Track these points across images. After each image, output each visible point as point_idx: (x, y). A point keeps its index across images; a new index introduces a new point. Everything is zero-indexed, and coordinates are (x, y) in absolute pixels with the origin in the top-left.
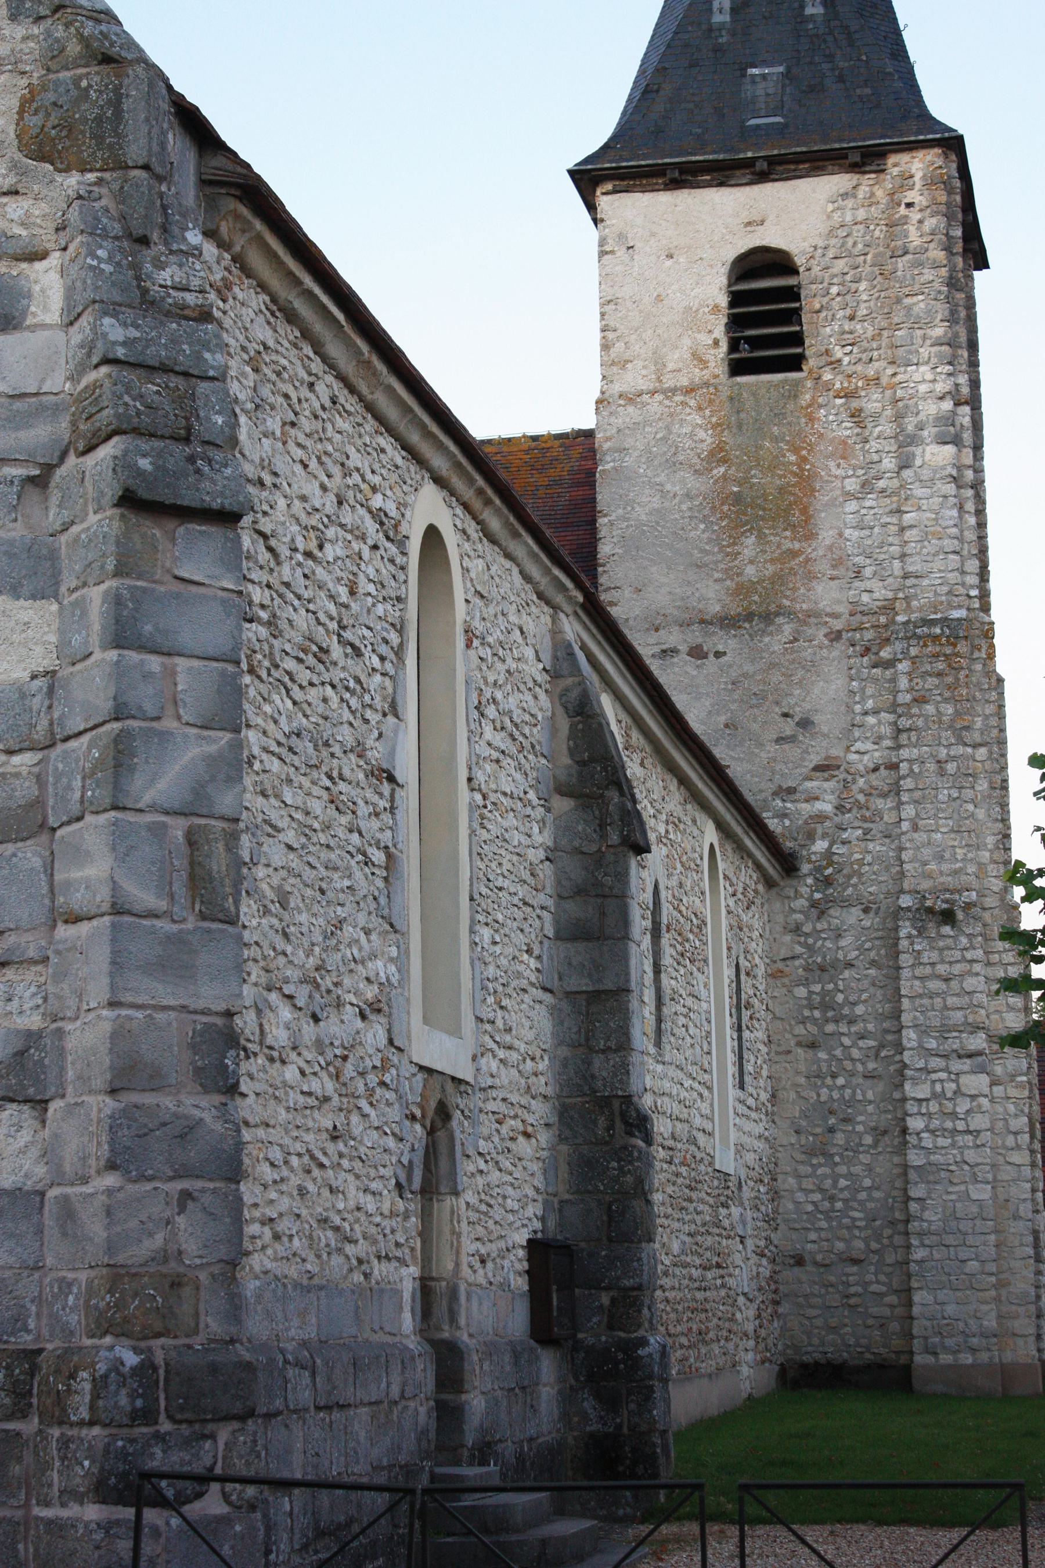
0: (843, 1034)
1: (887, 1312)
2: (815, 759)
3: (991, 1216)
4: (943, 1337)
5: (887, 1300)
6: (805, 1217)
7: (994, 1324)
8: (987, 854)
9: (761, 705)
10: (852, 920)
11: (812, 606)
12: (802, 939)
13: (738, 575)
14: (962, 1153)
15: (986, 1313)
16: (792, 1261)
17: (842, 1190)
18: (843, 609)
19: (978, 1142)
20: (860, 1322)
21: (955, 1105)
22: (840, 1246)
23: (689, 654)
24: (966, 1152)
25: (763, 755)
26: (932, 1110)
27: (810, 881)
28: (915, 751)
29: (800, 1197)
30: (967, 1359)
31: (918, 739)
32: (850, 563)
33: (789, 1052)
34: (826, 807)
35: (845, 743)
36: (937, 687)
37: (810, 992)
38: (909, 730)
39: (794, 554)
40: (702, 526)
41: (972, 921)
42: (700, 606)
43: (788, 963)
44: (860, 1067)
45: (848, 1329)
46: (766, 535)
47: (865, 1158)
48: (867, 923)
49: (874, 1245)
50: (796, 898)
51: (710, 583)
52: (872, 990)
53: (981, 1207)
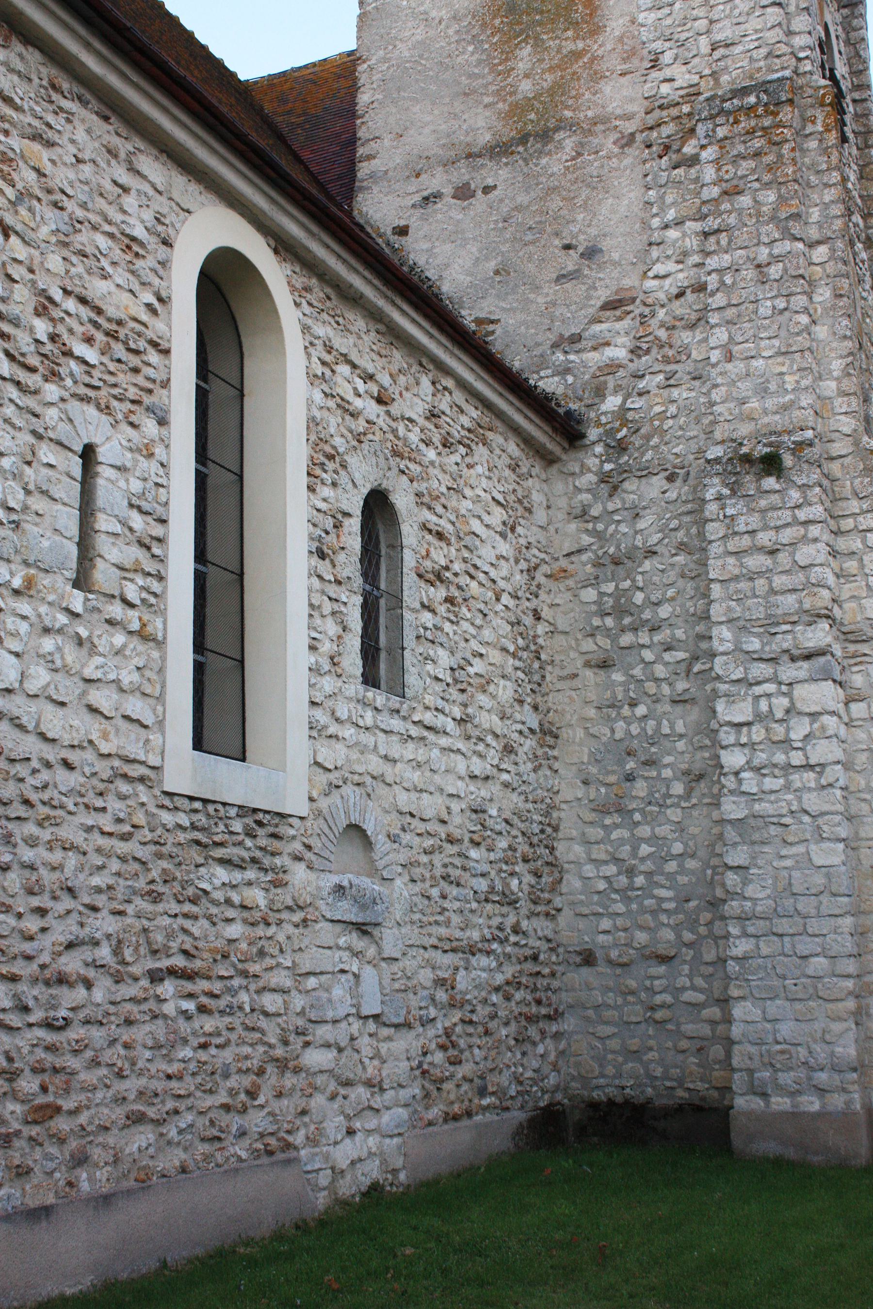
0: (643, 646)
1: (706, 1030)
2: (603, 295)
3: (843, 890)
4: (776, 1071)
5: (706, 1013)
6: (596, 898)
7: (852, 1052)
8: (833, 385)
9: (537, 240)
10: (654, 493)
11: (599, 111)
12: (590, 526)
13: (511, 94)
14: (800, 799)
15: (841, 1035)
16: (578, 959)
17: (643, 859)
18: (637, 108)
19: (823, 782)
20: (670, 1044)
21: (788, 730)
22: (641, 937)
23: (454, 197)
24: (806, 796)
25: (541, 300)
26: (756, 738)
27: (599, 449)
28: (727, 257)
29: (589, 870)
30: (812, 1104)
31: (730, 242)
32: (645, 52)
33: (575, 676)
34: (618, 353)
35: (643, 268)
36: (754, 171)
37: (601, 594)
38: (718, 231)
39: (577, 55)
40: (471, 48)
41: (805, 466)
42: (468, 139)
43: (573, 558)
44: (666, 689)
45: (651, 1055)
46: (543, 40)
47: (674, 814)
48: (672, 495)
49: (688, 936)
50: (582, 473)
51: (480, 110)
52: (681, 583)
53: (828, 876)
